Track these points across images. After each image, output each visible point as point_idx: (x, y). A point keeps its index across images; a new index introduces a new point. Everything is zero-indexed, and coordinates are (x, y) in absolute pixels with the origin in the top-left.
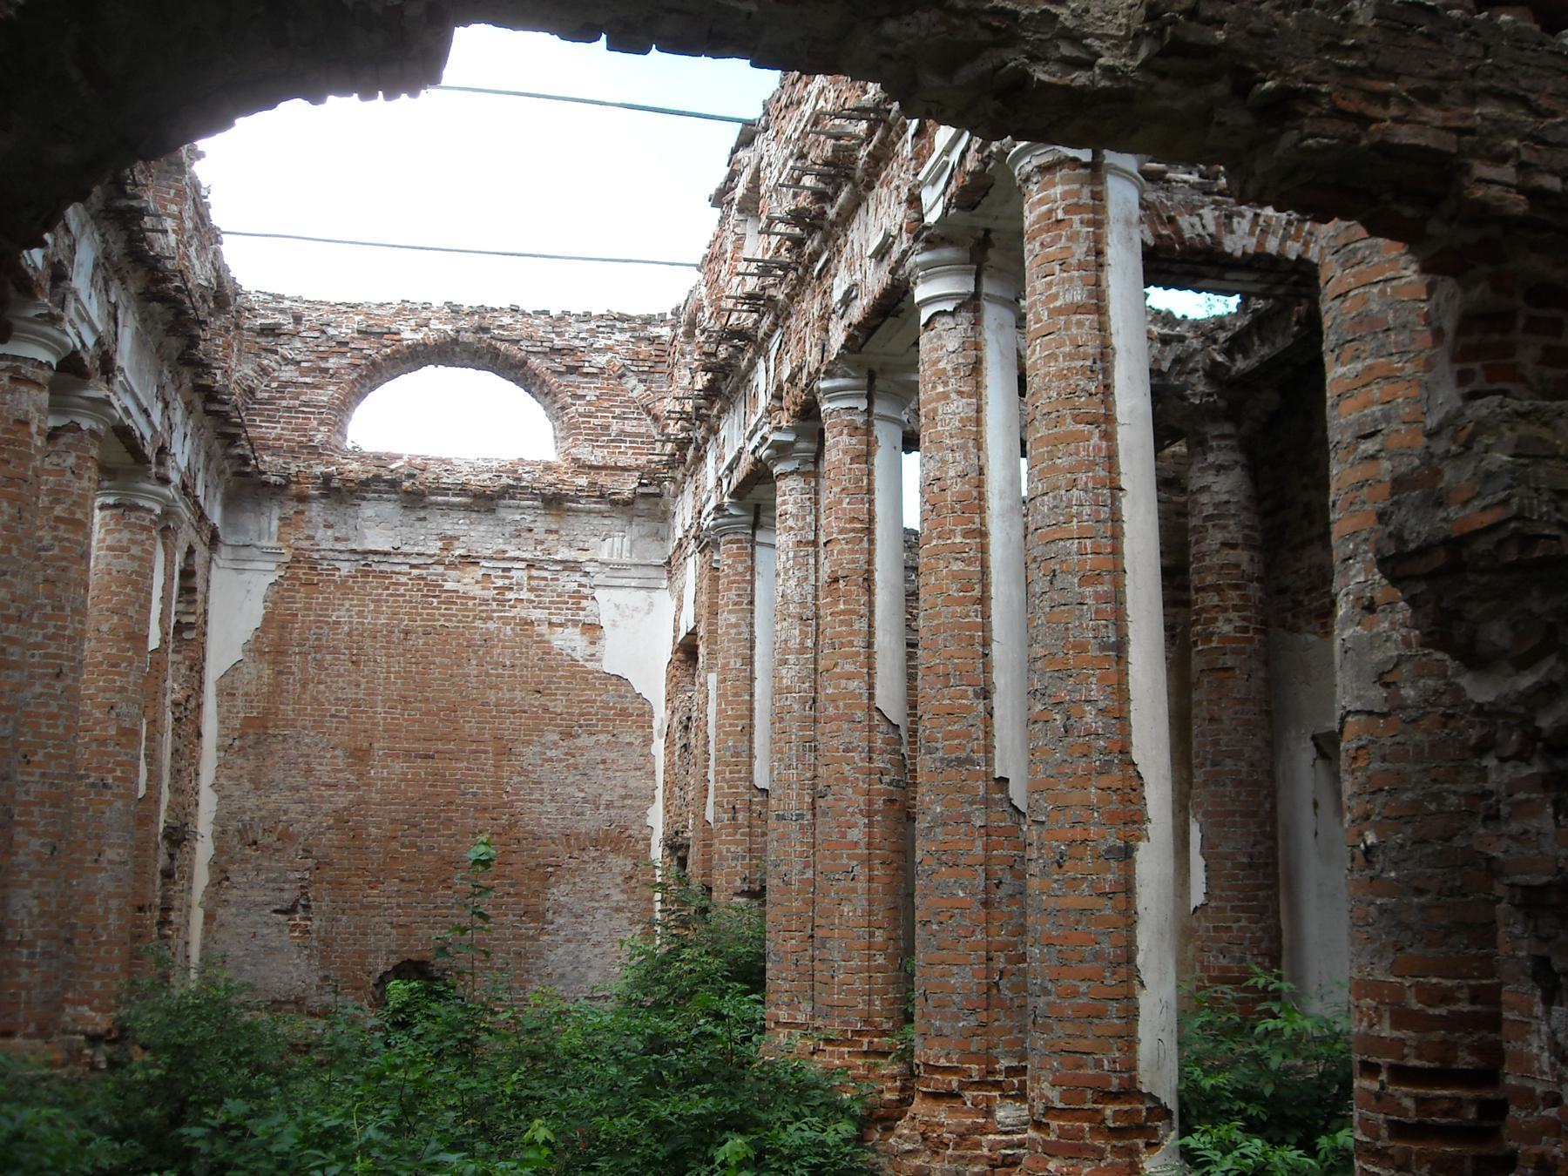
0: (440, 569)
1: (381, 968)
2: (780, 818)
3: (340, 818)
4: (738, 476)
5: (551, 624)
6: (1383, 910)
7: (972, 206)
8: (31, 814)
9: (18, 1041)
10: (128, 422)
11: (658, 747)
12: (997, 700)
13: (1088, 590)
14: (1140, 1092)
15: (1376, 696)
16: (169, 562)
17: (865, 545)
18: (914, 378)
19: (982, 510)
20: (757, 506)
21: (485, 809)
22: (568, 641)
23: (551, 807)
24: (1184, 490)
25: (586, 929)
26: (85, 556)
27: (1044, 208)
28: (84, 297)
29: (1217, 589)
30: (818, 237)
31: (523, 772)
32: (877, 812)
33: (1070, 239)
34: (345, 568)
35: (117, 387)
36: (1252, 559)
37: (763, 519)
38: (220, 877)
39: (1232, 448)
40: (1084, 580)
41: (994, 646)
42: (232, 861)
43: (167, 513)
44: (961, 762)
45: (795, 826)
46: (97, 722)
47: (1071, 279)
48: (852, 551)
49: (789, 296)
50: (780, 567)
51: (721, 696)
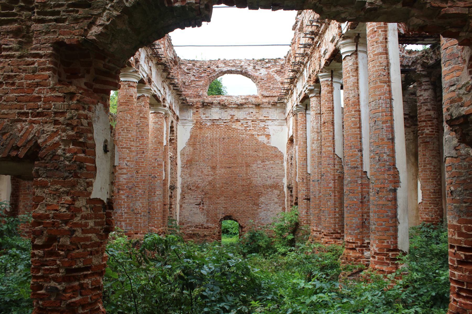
0: (230, 123)
1: (221, 218)
2: (313, 181)
3: (210, 183)
4: (301, 97)
5: (258, 135)
6: (455, 207)
7: (354, 28)
8: (139, 184)
9: (139, 235)
10: (155, 93)
11: (285, 164)
12: (364, 152)
13: (384, 125)
14: (398, 249)
15: (454, 153)
16: (167, 125)
17: (332, 114)
18: (341, 71)
19: (359, 105)
20: (306, 105)
21: (244, 180)
22: (262, 139)
23: (260, 179)
24: (416, 96)
25: (269, 208)
26: (148, 125)
27: (371, 28)
28: (143, 66)
29: (424, 121)
30: (317, 37)
31: (253, 171)
32: (336, 180)
33: (378, 36)
34: (209, 124)
35: (152, 86)
36: (434, 113)
37: (308, 108)
38: (183, 197)
39: (429, 84)
40: (383, 123)
41: (363, 139)
42: (185, 193)
43: (166, 114)
44: (355, 168)
45: (317, 183)
46: (153, 163)
47: (379, 46)
48: (329, 116)
49: (312, 53)
50: (312, 120)
51: (299, 151)
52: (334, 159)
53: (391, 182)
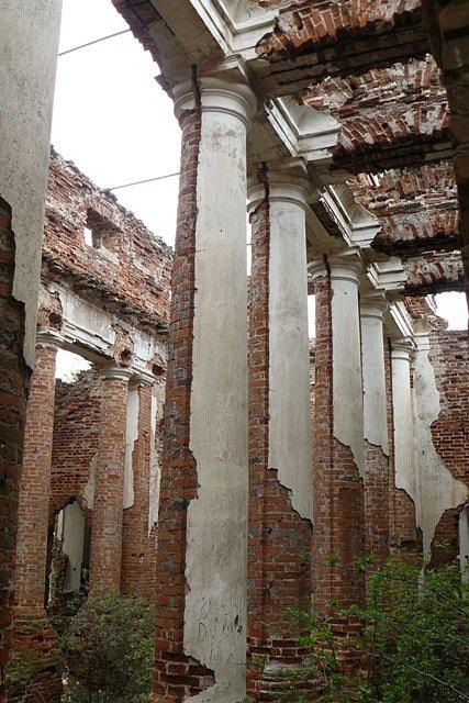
52: (332, 449)
53: (177, 484)
